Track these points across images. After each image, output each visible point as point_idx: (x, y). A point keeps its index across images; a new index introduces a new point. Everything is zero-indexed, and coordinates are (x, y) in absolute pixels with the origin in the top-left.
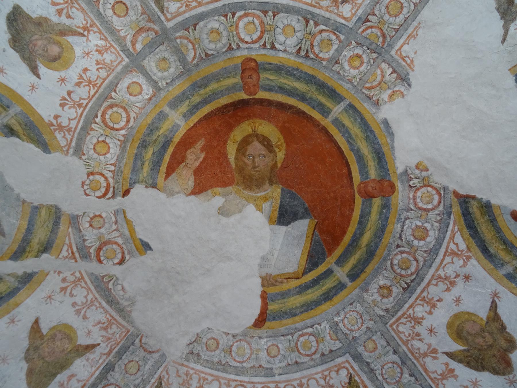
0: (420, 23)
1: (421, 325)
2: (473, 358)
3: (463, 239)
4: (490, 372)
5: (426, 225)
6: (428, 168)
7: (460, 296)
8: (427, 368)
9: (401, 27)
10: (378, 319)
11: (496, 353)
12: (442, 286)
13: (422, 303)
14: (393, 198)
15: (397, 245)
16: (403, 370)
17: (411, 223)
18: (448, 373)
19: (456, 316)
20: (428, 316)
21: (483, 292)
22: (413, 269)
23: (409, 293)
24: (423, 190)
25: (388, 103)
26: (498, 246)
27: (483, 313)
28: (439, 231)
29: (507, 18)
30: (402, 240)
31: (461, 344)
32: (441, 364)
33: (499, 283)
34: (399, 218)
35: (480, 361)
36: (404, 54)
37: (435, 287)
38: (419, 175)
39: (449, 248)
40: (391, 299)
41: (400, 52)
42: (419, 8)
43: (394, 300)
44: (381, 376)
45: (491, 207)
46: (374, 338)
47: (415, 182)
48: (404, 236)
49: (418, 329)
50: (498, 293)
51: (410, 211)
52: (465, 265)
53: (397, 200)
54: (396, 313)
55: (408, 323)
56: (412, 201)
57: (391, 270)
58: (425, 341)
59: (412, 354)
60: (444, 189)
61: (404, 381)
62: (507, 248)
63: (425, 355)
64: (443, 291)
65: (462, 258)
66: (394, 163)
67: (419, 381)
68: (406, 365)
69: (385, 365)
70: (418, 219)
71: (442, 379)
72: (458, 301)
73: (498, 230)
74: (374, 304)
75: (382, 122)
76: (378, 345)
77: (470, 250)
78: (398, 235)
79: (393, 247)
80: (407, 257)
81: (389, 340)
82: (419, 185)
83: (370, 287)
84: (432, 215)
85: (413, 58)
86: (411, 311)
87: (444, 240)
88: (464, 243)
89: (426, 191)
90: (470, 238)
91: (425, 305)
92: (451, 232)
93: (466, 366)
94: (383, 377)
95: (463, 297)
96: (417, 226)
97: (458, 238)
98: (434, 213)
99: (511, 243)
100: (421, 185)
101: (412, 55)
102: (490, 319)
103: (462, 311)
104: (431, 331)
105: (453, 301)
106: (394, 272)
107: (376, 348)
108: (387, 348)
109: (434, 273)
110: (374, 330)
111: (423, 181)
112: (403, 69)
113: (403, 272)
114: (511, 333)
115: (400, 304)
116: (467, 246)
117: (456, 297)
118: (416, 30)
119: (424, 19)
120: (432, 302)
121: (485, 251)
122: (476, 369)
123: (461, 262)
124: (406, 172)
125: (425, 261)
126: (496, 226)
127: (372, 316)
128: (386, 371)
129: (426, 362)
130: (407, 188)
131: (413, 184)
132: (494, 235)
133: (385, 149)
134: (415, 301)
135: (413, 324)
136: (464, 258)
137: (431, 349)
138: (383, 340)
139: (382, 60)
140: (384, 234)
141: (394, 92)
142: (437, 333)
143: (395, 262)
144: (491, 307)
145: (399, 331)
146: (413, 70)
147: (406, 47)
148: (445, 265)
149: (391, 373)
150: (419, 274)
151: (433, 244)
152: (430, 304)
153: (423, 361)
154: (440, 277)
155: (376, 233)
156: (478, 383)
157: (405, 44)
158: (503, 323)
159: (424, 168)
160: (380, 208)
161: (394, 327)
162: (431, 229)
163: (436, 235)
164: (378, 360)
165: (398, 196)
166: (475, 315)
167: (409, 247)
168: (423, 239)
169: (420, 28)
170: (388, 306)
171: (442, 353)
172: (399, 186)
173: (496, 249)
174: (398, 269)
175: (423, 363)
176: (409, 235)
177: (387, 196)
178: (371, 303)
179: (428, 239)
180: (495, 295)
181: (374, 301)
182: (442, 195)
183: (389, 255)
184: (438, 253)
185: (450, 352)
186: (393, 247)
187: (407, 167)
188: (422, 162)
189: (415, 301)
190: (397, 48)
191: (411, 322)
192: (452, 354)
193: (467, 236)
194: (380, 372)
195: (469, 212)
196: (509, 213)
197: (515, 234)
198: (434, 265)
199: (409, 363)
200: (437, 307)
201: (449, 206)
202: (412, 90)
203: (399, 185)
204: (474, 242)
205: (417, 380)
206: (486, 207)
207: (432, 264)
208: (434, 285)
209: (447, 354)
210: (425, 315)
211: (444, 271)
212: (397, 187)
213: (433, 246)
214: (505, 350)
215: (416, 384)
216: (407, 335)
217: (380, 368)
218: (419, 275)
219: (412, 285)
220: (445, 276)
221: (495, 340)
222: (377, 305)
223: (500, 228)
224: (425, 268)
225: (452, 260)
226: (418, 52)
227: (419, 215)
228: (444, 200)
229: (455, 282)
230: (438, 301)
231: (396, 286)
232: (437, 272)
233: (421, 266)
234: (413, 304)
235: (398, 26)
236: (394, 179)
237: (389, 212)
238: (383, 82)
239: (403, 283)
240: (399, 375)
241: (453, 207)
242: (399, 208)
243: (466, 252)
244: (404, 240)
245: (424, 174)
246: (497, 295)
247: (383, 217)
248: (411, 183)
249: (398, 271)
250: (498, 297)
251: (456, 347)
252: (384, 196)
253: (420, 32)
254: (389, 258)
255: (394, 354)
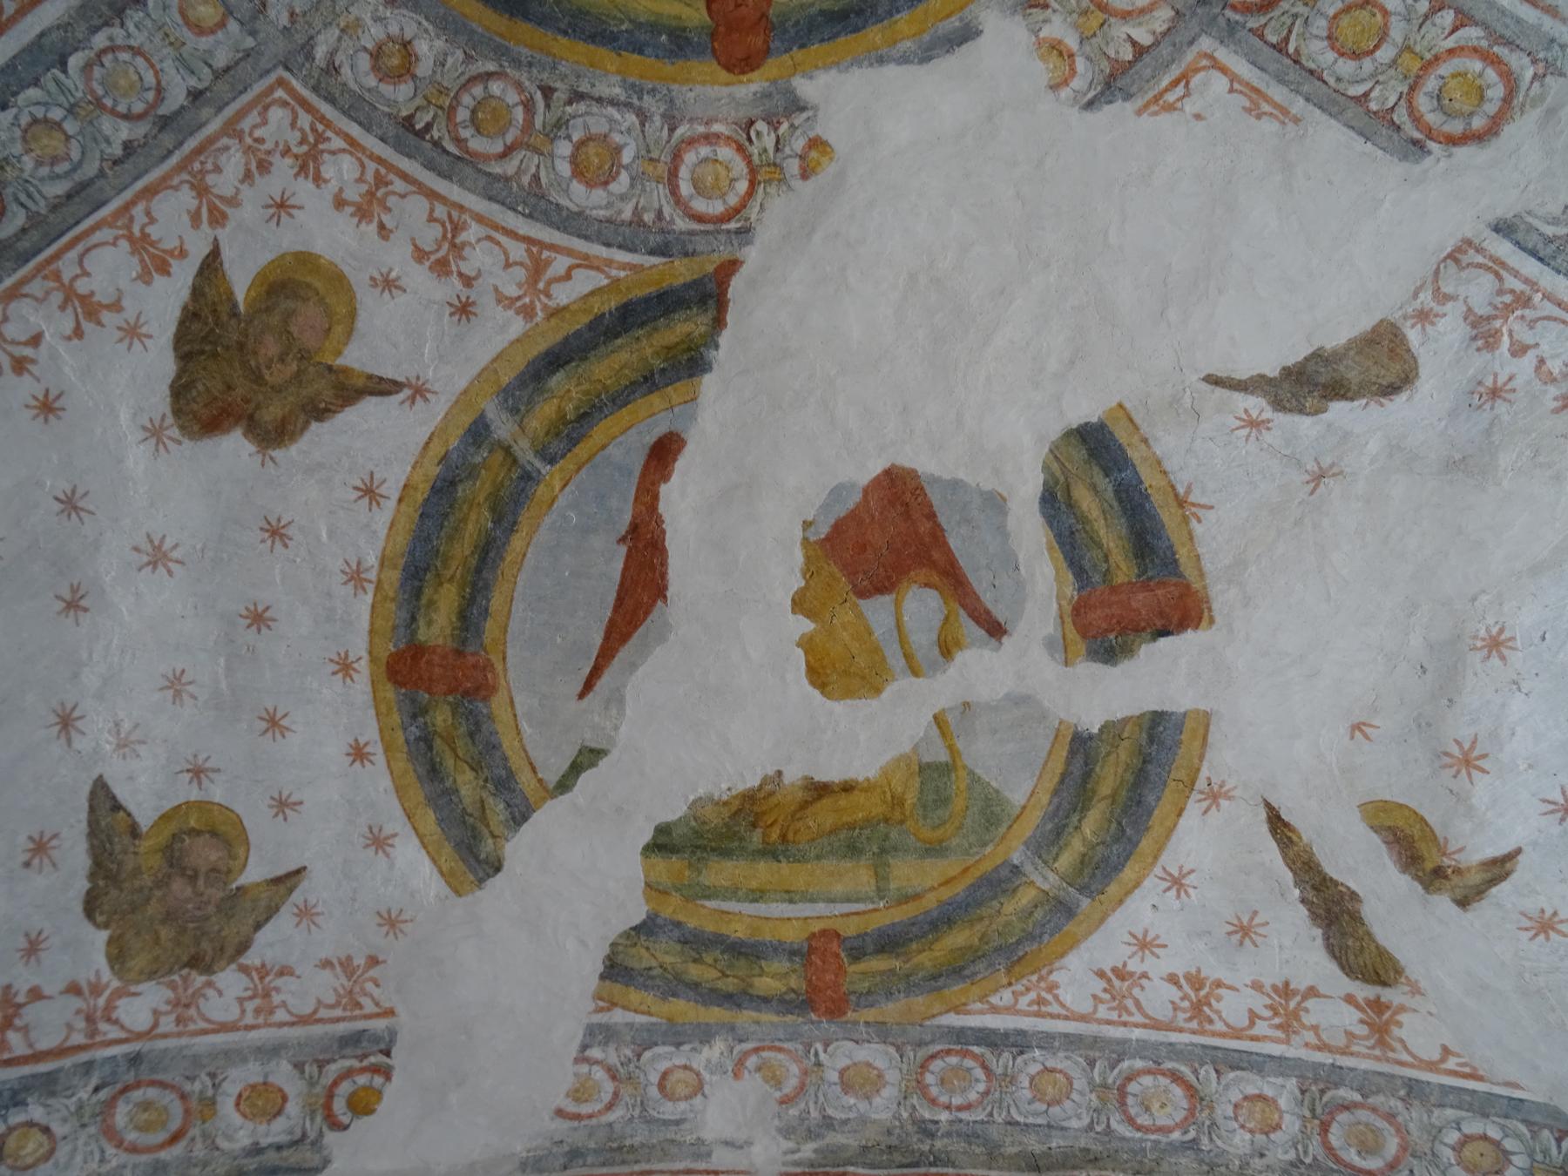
0: (1296, 120)
1: (297, 175)
2: (212, 330)
3: (587, 296)
4: (178, 377)
5: (624, 177)
6: (813, 178)
7: (405, 291)
8: (161, 195)
9: (1289, 62)
10: (300, 38)
11: (240, 391)
12: (430, 236)
13: (370, 176)
14: (710, 67)
15: (550, 88)
16: (140, 123)
17: (629, 131)
18: (152, 257)
19: (338, 280)
20: (330, 198)
21: (423, 355)
22: (477, 144)
23: (397, 136)
24: (740, 167)
25: (1034, 39)
26: (570, 399)
27: (356, 357)
28: (607, 221)
29: (1286, 386)
30: (570, 103)
31: (253, 293)
32: (180, 237)
33: (457, 402)
34: (642, 90)
35: (208, 348)
36: (1196, 80)
37: (425, 216)
38: (787, 151)
39: (553, 255)
40: (371, 81)
41: (1204, 68)
42: (1349, 114)
43: (369, 90)
44: (108, 43)
45: (691, 376)
46: (233, 26)
47: (766, 137)
48: (581, 107)
49: (283, 167)
50: (426, 400)
51: (666, 127)
52: (500, 298)
53: (704, 83)
54: (326, 99)
55: (298, 134)
56: (701, 129)
57: (467, 77)
58: (244, 187)
59: (199, 151)
60: (745, 233)
61: (106, 124)
62: (566, 423)
63: (201, 190)
64: (413, 239)
65: (525, 295)
66: (827, 67)
67: (111, 169)
68: (160, 131)
69: (147, 60)
70: (643, 152)
71: (130, 238)
72: (389, 284)
73: (621, 398)
74: (347, 26)
75: (967, 25)
76: (211, 39)
77: (552, 315)
78: (584, 87)
79: (545, 76)
80: (514, 122)
81: (233, 76)
82: (754, 150)
83: (405, 12)
84: (658, 195)
85: (1182, 110)
86: (337, 143)
87: (579, 236)
88: (572, 299)
89: (733, 174)
90: (591, 317)
91: (364, 188)
92: (605, 260)
93: (185, 308)
94: (104, 51)
95: (402, 299)
96: (618, 150)
97: (586, 281)
98: (664, 202)
99: (584, 436)
100: (756, 159)
101: (1190, 107)
102: (341, 377)
103: (358, 296)
104: (282, 206)
105: (384, 270)
106: (464, 87)
107: (199, 30)
108: (206, 70)
109: (470, 211)
110: (259, 25)
111: (769, 165)
112: (1148, 81)
113: (462, 115)
114: (307, 436)
115: (357, 107)
116: (565, 308)
117: (398, 278)
118: (1275, 112)
119: (1311, 130)
120: (376, 209)
121: (555, 360)
122: (180, 338)
123: (512, 291)
124: (796, 105)
125: (507, 179)
126: (634, 393)
127: (308, 18)
128: (125, 62)
129: (179, 193)
130: (743, 114)
131: (758, 134)
132: (605, 387)
133: (874, 34)
134: (372, 157)
135: (295, 150)
136: (527, 300)
137: (222, 207)
138: (231, 55)
139: (1183, 10)
140: (585, 41)
141: (1071, 56)
142: (278, 224)
143: (496, 87)
144: (381, 379)
145: (266, 108)
146: (1139, 113)
147: (1220, 83)
148: (498, 243)
149: (122, 82)
150: (461, 165)
151: (564, 202)
152: (370, 203)
153: (182, 182)
154: (457, 228)
155: (588, 13)
156: (136, 341)
157: (1232, 81)
158: (335, 412)
159: (812, 165)
160: (674, 23)
161: (280, 93)
162: (610, 194)
163: (594, 212)
164: (160, 35)
165: (714, 82)
166: (349, 333)
167: (548, 128)
168: (579, 171)
169: (1283, 123)
170: (346, 71)
171: (216, 239)
172: (750, 87)
173: (561, 393)
174: (474, 98)
175: (175, 181)
176: (586, 126)
177: (716, 44)
178: (352, 17)
179: (577, 188)
180: (419, 392)
181: (359, 26)
182: (724, 227)
183: (516, 63)
184: (537, 220)
185: (221, 264)
186: (545, 76)
187: (815, 108)
188: (831, 159)
189: (372, 157)
190: (1222, 54)
191: (301, 143)
192: (216, 270)
193: (596, 306)
194: (119, 42)
195: (674, 311)
196: (677, 427)
197: (611, 447)
198: (495, 207)
199: (167, 139)
200: (360, 222)
201: (690, 248)
202: (1074, 114)
203: (754, 87)
204: (579, 327)
205: (115, 163)
206: (691, 359)
207: (498, 202)
208: (432, 211)
209: (215, 254)
210: (333, 186)
211: (479, 240)
212: (744, 78)
213: (557, 205)
214: (251, 417)
215: (102, 160)
216: (258, 133)
217: (132, 42)
218: (458, 164)
219: (424, 143)
220: (464, 244)
221: (280, 391)
222: (345, 37)
223: (630, 403)
224: (482, 181)
225: (516, 263)
226: (1201, 124)
227: (655, 155)
228: (707, 233)
229: (448, 273)
230: (382, 226)
231: (415, 95)
232: (473, 219)
233: (488, 170)
234: (363, 150)
235: (1297, 50)
236: (772, 67)
237: (661, 54)
238: (1106, 16)
239: (428, 117)
240: (122, 108)
241: (686, 260)
242: (675, 87)
243: (545, 307)
244: (569, 109)
245: (793, 166)
246: (418, 397)
247: (642, 37)
248: (761, 126)
249: (466, 99)
250: (413, 400)
251: (241, 280)
252: (713, 35)
253: (1269, 126)
254: (506, 64)
255: (189, 93)
